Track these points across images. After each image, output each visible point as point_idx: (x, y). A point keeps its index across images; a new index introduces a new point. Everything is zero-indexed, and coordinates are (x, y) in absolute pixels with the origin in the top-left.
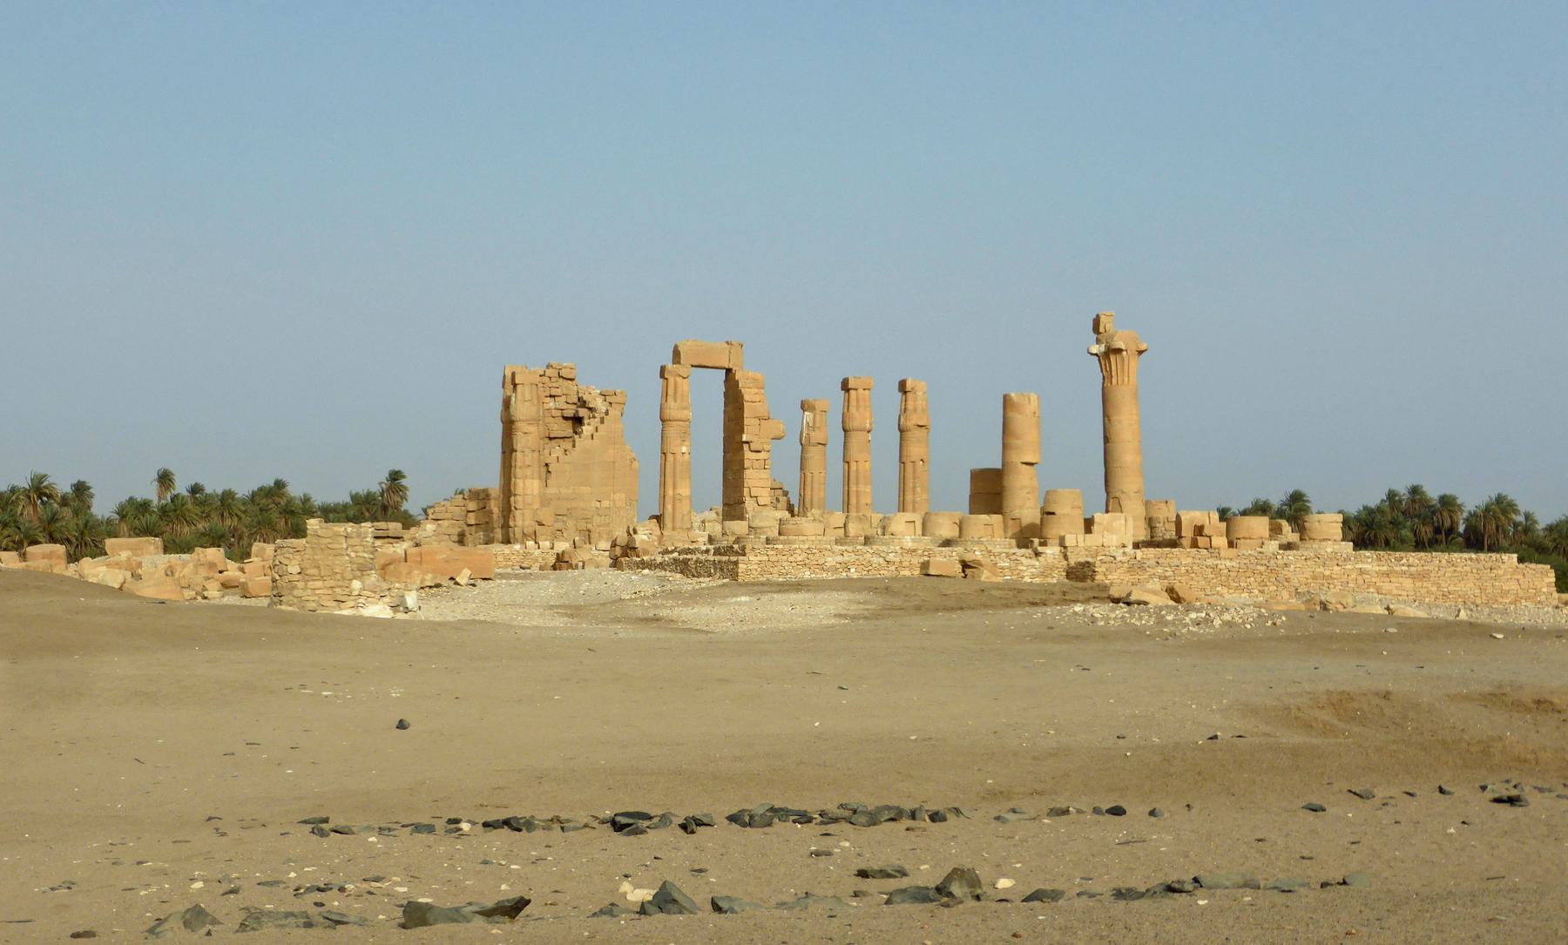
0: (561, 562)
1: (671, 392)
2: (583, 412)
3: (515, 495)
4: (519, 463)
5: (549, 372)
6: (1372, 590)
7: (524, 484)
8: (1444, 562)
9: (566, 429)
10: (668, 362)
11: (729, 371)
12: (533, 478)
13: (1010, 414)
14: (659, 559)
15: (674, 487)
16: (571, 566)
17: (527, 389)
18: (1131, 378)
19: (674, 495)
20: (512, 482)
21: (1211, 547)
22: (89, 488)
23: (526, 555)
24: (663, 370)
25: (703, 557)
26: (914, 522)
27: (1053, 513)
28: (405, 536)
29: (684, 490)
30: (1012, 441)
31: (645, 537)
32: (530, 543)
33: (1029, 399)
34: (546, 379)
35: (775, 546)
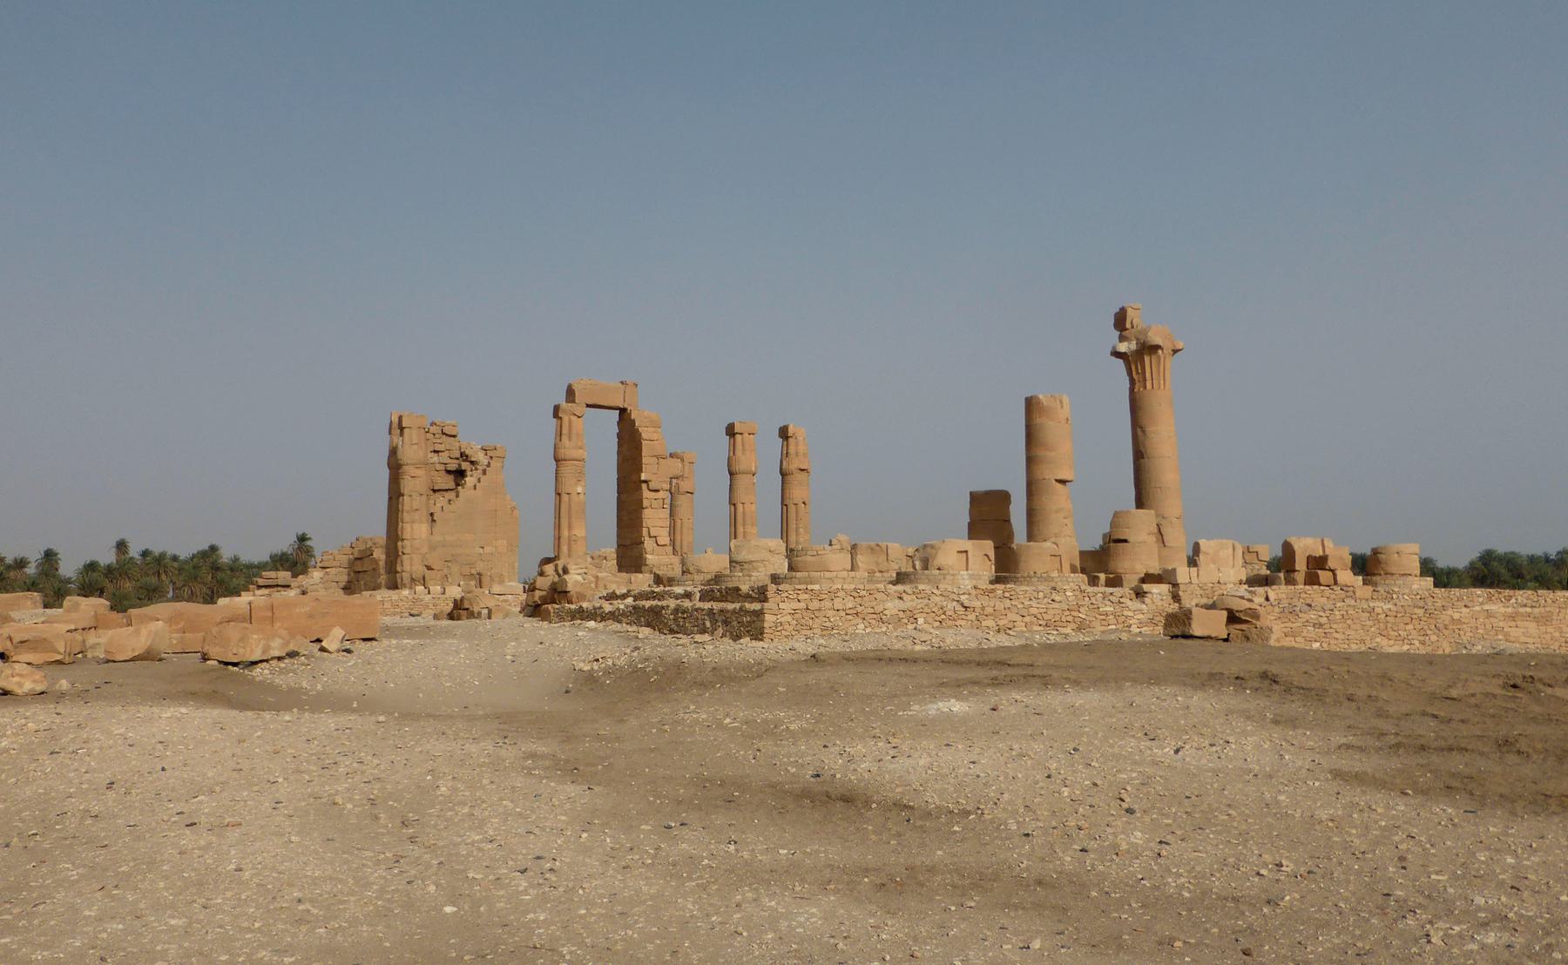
0: (459, 610)
1: (565, 431)
2: (465, 466)
3: (403, 540)
4: (406, 508)
5: (433, 429)
6: (1500, 637)
7: (412, 529)
8: (1549, 601)
9: (449, 482)
10: (561, 399)
11: (623, 411)
12: (421, 522)
13: (1038, 420)
14: (607, 607)
15: (570, 528)
16: (471, 615)
17: (415, 433)
18: (1167, 383)
19: (569, 537)
20: (400, 527)
21: (1336, 583)
22: (56, 554)
23: (415, 601)
24: (557, 409)
25: (687, 604)
26: (966, 552)
27: (1125, 541)
28: (292, 584)
29: (579, 532)
30: (1040, 452)
31: (579, 578)
32: (420, 588)
33: (1061, 402)
34: (430, 436)
35: (810, 587)
